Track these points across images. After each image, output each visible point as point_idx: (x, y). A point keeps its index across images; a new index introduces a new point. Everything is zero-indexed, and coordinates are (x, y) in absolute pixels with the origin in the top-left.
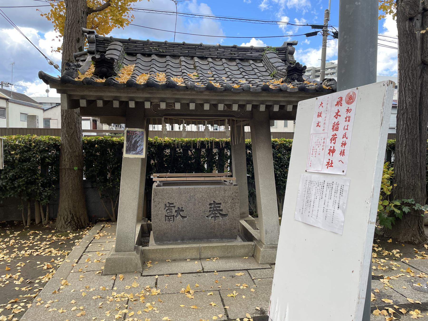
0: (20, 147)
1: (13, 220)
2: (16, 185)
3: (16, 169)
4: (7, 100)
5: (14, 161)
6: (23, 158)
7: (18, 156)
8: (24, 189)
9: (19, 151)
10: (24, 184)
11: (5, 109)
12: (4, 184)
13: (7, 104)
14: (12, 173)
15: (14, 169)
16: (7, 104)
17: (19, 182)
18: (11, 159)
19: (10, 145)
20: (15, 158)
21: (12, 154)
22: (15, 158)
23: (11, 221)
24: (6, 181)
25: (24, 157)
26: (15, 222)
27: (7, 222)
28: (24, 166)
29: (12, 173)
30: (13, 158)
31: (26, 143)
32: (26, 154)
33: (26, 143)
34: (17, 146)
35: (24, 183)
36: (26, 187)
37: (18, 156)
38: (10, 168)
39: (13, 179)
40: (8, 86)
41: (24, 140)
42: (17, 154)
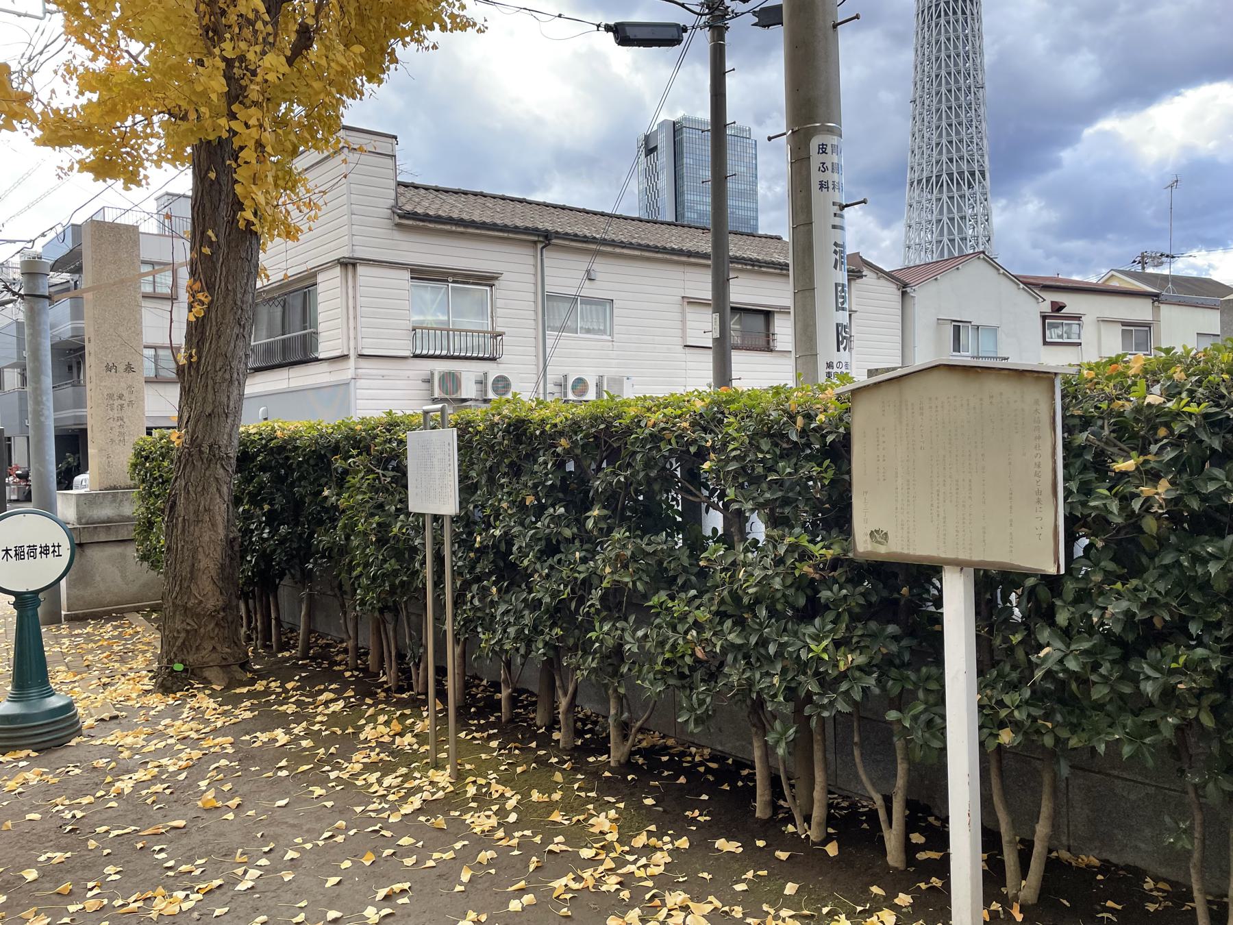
0: (1178, 428)
1: (1140, 864)
2: (1149, 688)
3: (1151, 575)
4: (1155, 298)
5: (1134, 522)
6: (1195, 504)
7: (1163, 490)
8: (1207, 721)
9: (1170, 454)
10: (1200, 694)
11: (1148, 325)
12: (1072, 665)
13: (1156, 310)
14: (1124, 604)
15: (1138, 572)
16: (1156, 310)
17: (1172, 672)
18: (1114, 506)
19: (1110, 413)
20: (1136, 505)
21: (1123, 474)
22: (1136, 505)
23: (1127, 868)
24: (1086, 645)
25: (1204, 498)
26: (1149, 884)
27: (1106, 867)
28: (1204, 562)
29: (1124, 604)
30: (1125, 499)
31: (1216, 398)
32: (1217, 472)
33: (1216, 398)
34: (1154, 418)
35: (1201, 681)
36: (1215, 710)
37: (1163, 490)
38: (1111, 566)
39: (1139, 639)
40: (1162, 263)
41: (1206, 373)
42: (1154, 477)
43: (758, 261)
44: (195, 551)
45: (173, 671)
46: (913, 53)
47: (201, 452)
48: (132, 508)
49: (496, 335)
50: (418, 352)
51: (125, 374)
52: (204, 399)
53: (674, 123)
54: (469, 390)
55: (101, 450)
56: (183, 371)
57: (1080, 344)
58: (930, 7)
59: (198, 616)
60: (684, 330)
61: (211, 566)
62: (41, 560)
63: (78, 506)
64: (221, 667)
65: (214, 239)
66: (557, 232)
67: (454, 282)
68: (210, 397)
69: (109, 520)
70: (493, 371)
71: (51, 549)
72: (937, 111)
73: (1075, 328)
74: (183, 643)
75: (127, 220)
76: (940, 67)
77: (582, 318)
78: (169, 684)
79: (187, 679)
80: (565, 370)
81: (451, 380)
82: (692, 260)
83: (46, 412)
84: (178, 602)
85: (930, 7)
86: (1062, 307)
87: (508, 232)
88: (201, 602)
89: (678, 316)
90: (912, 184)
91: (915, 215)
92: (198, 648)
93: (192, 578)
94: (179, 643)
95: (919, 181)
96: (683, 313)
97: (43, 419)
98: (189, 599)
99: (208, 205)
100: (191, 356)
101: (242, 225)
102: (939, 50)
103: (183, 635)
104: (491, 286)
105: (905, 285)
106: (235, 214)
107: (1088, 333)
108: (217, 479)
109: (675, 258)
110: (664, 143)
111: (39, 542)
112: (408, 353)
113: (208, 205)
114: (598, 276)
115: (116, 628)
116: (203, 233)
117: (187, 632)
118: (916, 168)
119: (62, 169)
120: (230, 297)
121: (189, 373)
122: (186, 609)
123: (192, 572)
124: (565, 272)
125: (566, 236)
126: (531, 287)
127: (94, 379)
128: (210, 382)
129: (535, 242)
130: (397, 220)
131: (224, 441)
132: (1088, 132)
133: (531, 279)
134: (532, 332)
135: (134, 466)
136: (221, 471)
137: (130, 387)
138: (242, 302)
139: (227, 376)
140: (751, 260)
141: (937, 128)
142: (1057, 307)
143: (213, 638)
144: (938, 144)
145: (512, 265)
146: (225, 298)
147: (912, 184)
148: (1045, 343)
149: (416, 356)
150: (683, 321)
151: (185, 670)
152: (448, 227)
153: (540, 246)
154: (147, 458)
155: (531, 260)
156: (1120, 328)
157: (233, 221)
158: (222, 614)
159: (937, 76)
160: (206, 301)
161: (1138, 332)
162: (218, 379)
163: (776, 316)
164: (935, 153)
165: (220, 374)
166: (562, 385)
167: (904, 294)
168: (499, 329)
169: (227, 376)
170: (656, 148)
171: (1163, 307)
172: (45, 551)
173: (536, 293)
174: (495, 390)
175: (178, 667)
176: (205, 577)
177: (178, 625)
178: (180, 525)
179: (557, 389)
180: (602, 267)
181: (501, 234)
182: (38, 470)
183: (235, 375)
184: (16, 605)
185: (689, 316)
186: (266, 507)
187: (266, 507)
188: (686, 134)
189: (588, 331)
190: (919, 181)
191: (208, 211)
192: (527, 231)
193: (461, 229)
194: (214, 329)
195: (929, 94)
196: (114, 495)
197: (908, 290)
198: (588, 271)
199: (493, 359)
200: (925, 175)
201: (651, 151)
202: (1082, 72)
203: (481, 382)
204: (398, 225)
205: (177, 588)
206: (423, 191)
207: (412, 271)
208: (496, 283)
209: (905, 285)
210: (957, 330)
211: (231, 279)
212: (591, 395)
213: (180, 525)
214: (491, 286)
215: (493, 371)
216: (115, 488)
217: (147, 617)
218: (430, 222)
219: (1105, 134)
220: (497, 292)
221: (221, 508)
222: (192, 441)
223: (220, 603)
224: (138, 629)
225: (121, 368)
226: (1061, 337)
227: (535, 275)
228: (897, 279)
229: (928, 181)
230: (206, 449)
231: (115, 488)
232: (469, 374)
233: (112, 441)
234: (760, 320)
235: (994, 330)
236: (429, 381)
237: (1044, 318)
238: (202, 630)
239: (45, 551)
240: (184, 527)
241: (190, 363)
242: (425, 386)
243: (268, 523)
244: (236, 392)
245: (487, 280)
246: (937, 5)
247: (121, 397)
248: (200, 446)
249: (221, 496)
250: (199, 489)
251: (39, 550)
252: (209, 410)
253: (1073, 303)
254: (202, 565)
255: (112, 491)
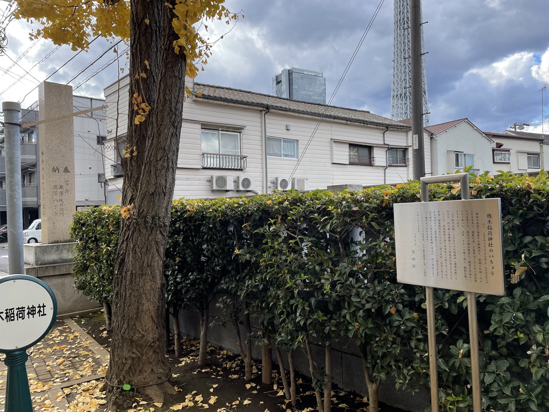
11: (538, 154)
13: (541, 147)
43: (366, 121)
44: (140, 297)
45: (123, 390)
46: (393, 39)
47: (146, 222)
48: (72, 254)
49: (243, 157)
50: (205, 166)
51: (64, 174)
52: (148, 181)
53: (289, 71)
54: (230, 185)
55: (49, 219)
56: (126, 163)
57: (509, 163)
58: (400, 20)
59: (141, 346)
60: (332, 155)
61: (151, 308)
62: (29, 320)
63: (36, 254)
64: (158, 385)
65: (148, 67)
66: (272, 106)
67: (222, 130)
68: (153, 181)
69: (55, 262)
70: (242, 176)
71: (37, 310)
72: (404, 65)
73: (507, 156)
74: (130, 368)
75: (64, 83)
76: (405, 46)
77: (283, 149)
78: (120, 402)
79: (133, 397)
80: (276, 175)
81: (222, 180)
82: (336, 120)
83: (17, 196)
84: (126, 336)
85: (400, 20)
86: (501, 145)
87: (249, 105)
88: (143, 336)
89: (329, 149)
90: (393, 97)
91: (395, 110)
92: (140, 371)
93: (137, 318)
94: (126, 368)
95: (397, 96)
96: (331, 147)
97: (15, 200)
98: (134, 334)
99: (143, 43)
100: (132, 152)
101: (177, 50)
102: (405, 38)
103: (130, 362)
104: (240, 133)
105: (432, 134)
106: (171, 43)
107: (513, 158)
108: (157, 243)
109: (328, 119)
110: (284, 79)
111: (26, 304)
112: (200, 167)
113: (143, 43)
114: (291, 128)
115: (61, 332)
116: (142, 62)
117: (133, 359)
118: (395, 90)
119: (32, 35)
120: (167, 105)
121: (131, 164)
122: (132, 341)
123: (137, 314)
124: (276, 126)
125: (276, 108)
126: (260, 134)
127: (45, 177)
128: (153, 169)
129: (261, 111)
130: (194, 98)
131: (162, 214)
132: (466, 74)
133: (259, 129)
134: (259, 156)
135: (74, 229)
136: (160, 236)
137: (67, 181)
138: (176, 109)
139: (166, 165)
140: (363, 121)
141: (404, 72)
142: (499, 146)
143: (151, 363)
144: (405, 80)
145: (250, 122)
146: (163, 106)
147: (393, 97)
148: (494, 162)
149: (204, 168)
150: (332, 151)
151: (132, 390)
152: (219, 102)
153: (264, 113)
154: (83, 225)
155: (259, 120)
156: (526, 155)
157: (170, 48)
158: (157, 343)
159: (404, 50)
160: (147, 109)
161: (534, 158)
162: (159, 167)
163: (375, 149)
164: (403, 84)
165: (160, 163)
166: (275, 183)
167: (431, 138)
168: (244, 155)
169: (166, 165)
170: (280, 81)
171: (544, 145)
172: (32, 311)
173: (261, 136)
174: (243, 186)
175: (127, 387)
176: (146, 317)
177: (126, 354)
178: (128, 278)
179: (272, 185)
180: (294, 124)
181: (245, 106)
182: (12, 233)
183: (171, 164)
184: (6, 361)
185: (334, 148)
186: (178, 259)
187: (178, 259)
188: (294, 75)
189: (286, 156)
190: (397, 96)
191: (144, 48)
192: (258, 105)
193: (226, 103)
194: (155, 130)
195: (400, 57)
196: (58, 246)
197: (434, 136)
198: (287, 126)
199: (241, 170)
200: (399, 93)
201: (279, 82)
202: (462, 48)
203: (236, 182)
204: (194, 101)
205: (125, 326)
206: (202, 87)
207: (202, 125)
208: (242, 131)
209: (432, 134)
210: (457, 156)
211: (168, 92)
212: (289, 188)
213: (128, 278)
214: (240, 133)
215: (242, 176)
216: (58, 242)
217: (79, 322)
218: (211, 99)
219: (476, 77)
220: (243, 136)
221: (158, 263)
222: (139, 214)
223: (157, 336)
224: (77, 334)
225: (62, 170)
226: (501, 160)
227: (261, 127)
228: (428, 131)
229: (400, 96)
230: (149, 220)
231: (58, 242)
232: (230, 177)
233: (56, 214)
234: (366, 151)
235: (472, 156)
236: (210, 181)
237: (493, 150)
238: (144, 357)
239: (32, 311)
240: (131, 278)
241: (132, 157)
242: (208, 183)
243: (180, 271)
244: (170, 177)
245: (238, 129)
246: (403, 19)
247: (61, 187)
248: (145, 217)
249: (159, 255)
250: (144, 250)
251: (26, 311)
252: (152, 190)
253: (507, 144)
254: (145, 307)
255: (57, 244)
